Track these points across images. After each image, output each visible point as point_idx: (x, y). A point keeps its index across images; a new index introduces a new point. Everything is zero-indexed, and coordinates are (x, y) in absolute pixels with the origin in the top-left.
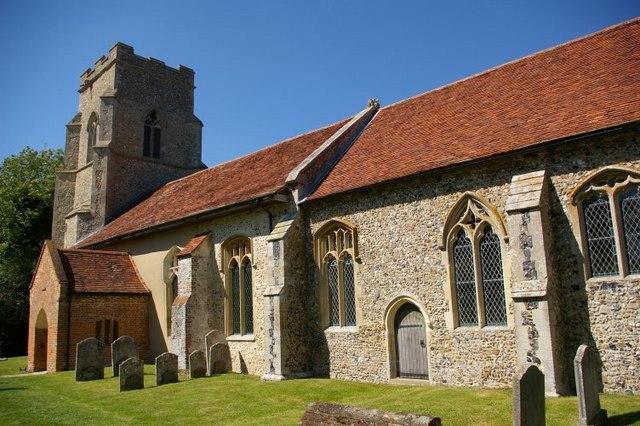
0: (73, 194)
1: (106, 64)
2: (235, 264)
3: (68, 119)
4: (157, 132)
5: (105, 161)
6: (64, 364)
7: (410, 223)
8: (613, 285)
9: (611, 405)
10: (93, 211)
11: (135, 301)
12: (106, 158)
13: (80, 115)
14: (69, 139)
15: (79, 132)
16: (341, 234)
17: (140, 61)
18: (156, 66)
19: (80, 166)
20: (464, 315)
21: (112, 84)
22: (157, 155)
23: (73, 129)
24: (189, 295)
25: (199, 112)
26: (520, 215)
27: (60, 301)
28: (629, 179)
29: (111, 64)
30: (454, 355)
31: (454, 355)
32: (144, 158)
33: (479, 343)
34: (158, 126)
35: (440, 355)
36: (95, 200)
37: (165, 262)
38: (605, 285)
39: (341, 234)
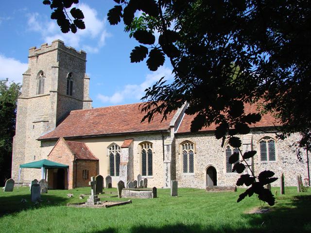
1: (50, 49)
2: (144, 151)
4: (72, 82)
6: (75, 186)
7: (214, 143)
8: (266, 163)
9: (189, 130)
16: (189, 144)
17: (66, 49)
18: (73, 50)
20: (185, 171)
22: (71, 95)
24: (128, 161)
26: (246, 145)
28: (271, 139)
29: (55, 50)
30: (225, 180)
31: (225, 180)
32: (67, 96)
33: (232, 177)
34: (72, 80)
35: (221, 181)
38: (264, 163)
39: (189, 144)
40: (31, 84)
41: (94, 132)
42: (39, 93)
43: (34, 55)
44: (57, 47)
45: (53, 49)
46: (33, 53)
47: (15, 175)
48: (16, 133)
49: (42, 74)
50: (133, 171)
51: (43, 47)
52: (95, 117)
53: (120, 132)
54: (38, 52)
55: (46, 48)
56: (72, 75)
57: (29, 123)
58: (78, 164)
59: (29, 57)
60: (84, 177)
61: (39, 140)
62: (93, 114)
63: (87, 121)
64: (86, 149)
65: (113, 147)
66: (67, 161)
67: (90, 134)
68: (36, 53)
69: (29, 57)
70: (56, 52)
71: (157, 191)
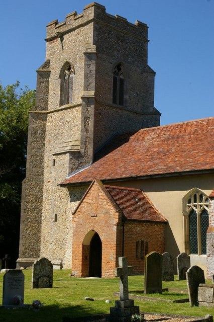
0: (44, 132)
1: (80, 22)
2: (192, 211)
3: (38, 65)
4: (122, 81)
5: (92, 108)
10: (83, 151)
11: (157, 228)
12: (92, 106)
13: (47, 64)
14: (39, 83)
15: (48, 77)
17: (110, 18)
18: (121, 22)
19: (51, 108)
21: (91, 41)
22: (121, 103)
23: (43, 75)
25: (151, 63)
27: (118, 225)
29: (88, 23)
34: (122, 77)
36: (84, 141)
37: (184, 199)
40: (51, 87)
41: (159, 169)
42: (61, 104)
43: (54, 35)
44: (92, 16)
45: (85, 21)
46: (53, 32)
47: (26, 249)
48: (27, 175)
49: (69, 69)
50: (85, 128)
51: (68, 19)
52: (163, 141)
53: (208, 167)
54: (62, 30)
55: (74, 21)
56: (122, 67)
57: (48, 158)
58: (126, 229)
59: (47, 40)
60: (139, 255)
61: (62, 185)
62: (159, 136)
63: (148, 149)
64: (145, 200)
65: (195, 196)
66: (106, 222)
67: (151, 173)
68: (57, 31)
69: (47, 40)
70: (91, 26)
71: (54, 271)
